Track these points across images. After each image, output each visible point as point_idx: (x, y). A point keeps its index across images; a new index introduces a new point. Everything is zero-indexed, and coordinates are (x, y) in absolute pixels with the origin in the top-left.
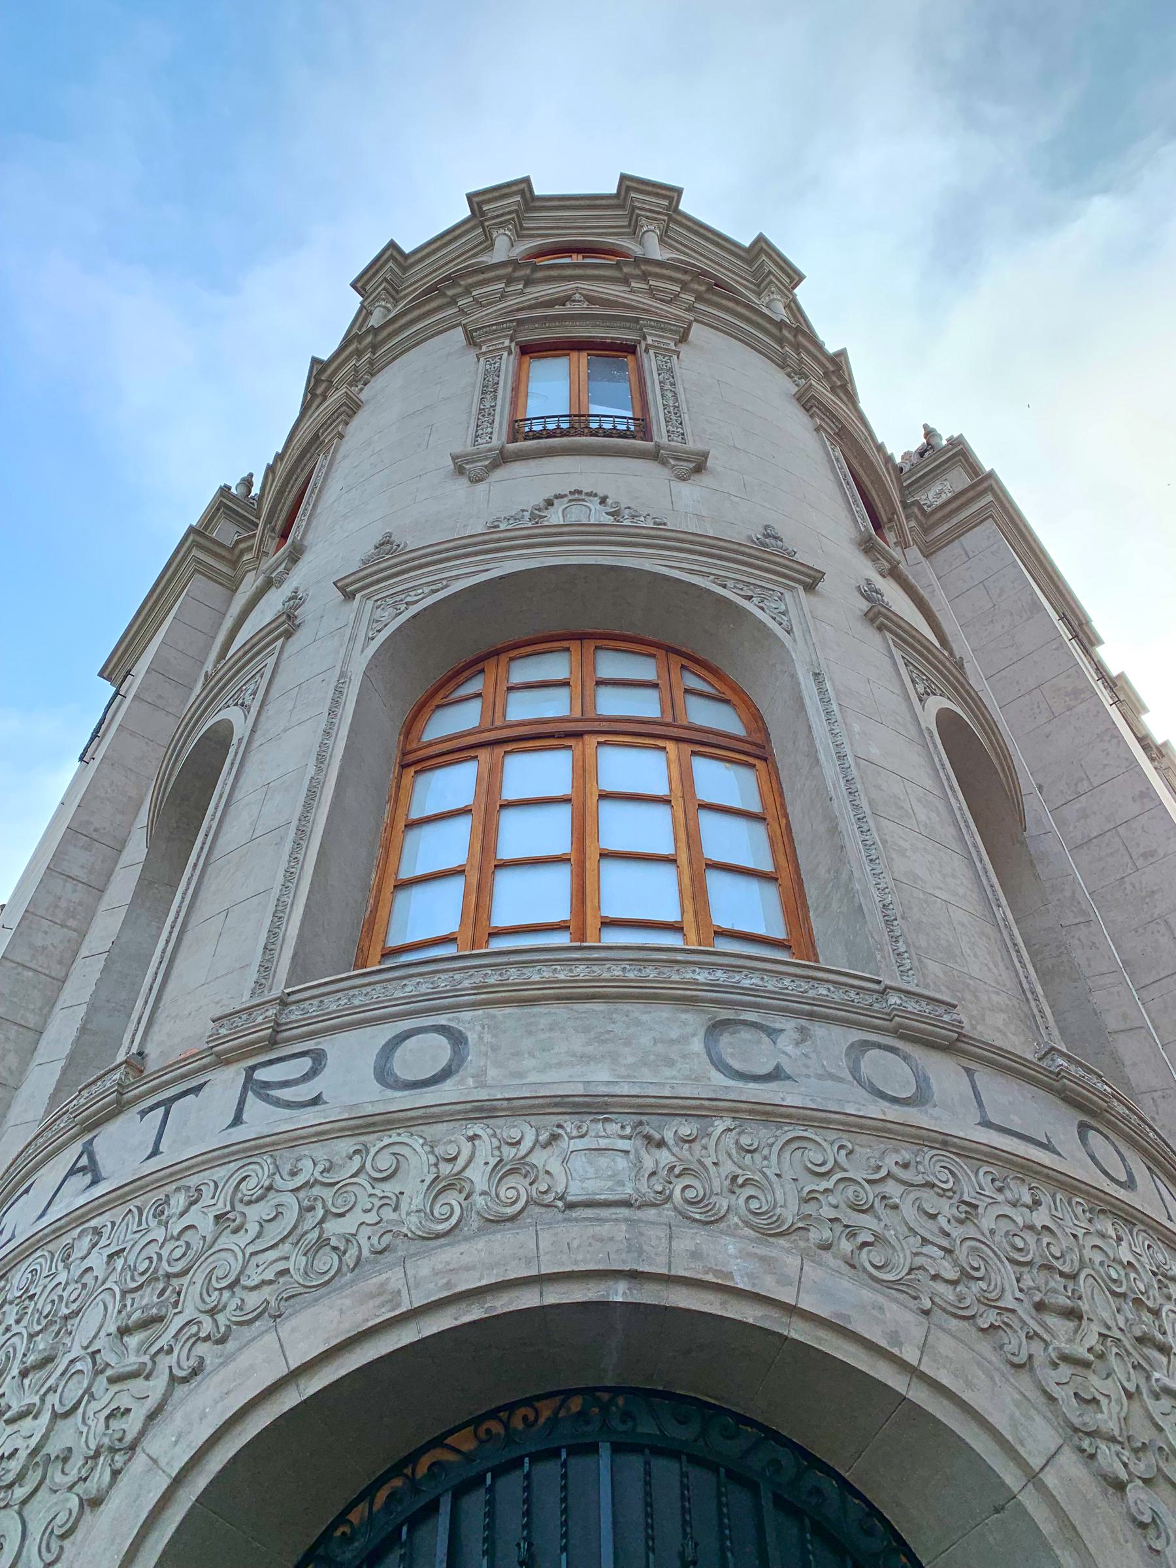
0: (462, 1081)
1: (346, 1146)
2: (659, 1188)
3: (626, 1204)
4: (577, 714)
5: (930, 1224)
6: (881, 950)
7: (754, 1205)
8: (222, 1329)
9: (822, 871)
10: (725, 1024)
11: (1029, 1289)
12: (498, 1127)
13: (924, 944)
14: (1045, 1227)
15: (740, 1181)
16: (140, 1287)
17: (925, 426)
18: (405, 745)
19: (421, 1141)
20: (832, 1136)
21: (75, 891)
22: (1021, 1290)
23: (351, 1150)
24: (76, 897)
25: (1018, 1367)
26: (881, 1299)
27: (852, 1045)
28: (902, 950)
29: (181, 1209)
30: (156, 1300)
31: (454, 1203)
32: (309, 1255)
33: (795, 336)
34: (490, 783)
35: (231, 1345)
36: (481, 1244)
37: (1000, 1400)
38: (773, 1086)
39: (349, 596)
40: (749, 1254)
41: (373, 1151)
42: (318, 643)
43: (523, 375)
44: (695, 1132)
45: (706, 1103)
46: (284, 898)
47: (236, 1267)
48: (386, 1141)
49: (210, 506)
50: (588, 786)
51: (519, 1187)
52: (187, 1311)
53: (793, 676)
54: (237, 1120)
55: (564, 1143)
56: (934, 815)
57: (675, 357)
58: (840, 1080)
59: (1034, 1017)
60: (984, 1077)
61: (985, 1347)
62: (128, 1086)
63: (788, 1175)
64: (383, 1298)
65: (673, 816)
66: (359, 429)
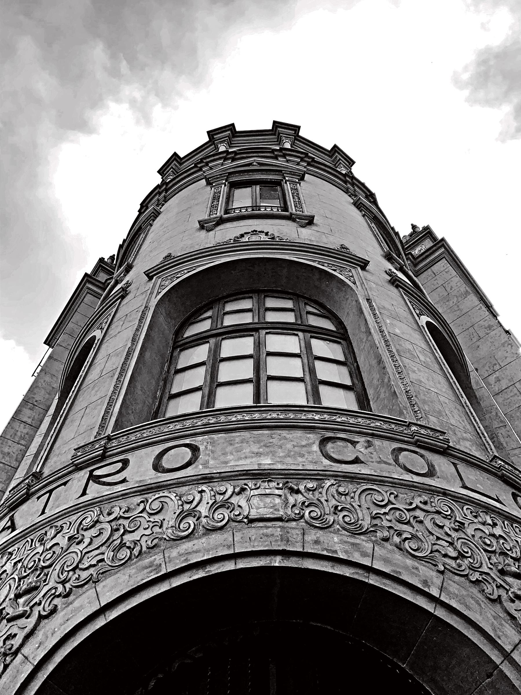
0: (196, 467)
1: (138, 499)
2: (297, 512)
3: (280, 519)
4: (256, 320)
5: (440, 531)
6: (406, 409)
7: (347, 519)
8: (68, 590)
9: (375, 382)
10: (329, 439)
11: (495, 563)
12: (214, 487)
13: (427, 409)
14: (500, 536)
15: (339, 508)
16: (28, 575)
17: (412, 225)
18: (175, 339)
19: (175, 495)
20: (387, 489)
21: (25, 428)
22: (491, 564)
23: (139, 501)
24: (25, 431)
25: (493, 601)
26: (416, 564)
27: (394, 449)
28: (416, 410)
29: (52, 535)
30: (35, 579)
31: (191, 522)
32: (115, 551)
33: (352, 180)
34: (215, 352)
35: (71, 598)
36: (204, 540)
37: (486, 617)
38: (355, 465)
39: (150, 278)
40: (346, 542)
41: (150, 501)
42: (136, 298)
43: (231, 194)
44: (315, 486)
45: (321, 472)
46: (113, 397)
47: (77, 560)
48: (157, 496)
49: (95, 267)
50: (261, 350)
51: (224, 513)
52: (51, 583)
53: (357, 301)
54: (84, 493)
55: (248, 492)
56: (428, 359)
57: (298, 185)
58: (390, 464)
59: (485, 445)
60: (461, 467)
61: (475, 590)
62: (33, 486)
63: (365, 505)
64: (154, 568)
65: (302, 362)
66: (158, 223)
